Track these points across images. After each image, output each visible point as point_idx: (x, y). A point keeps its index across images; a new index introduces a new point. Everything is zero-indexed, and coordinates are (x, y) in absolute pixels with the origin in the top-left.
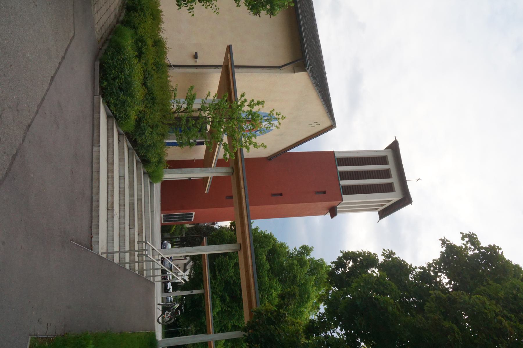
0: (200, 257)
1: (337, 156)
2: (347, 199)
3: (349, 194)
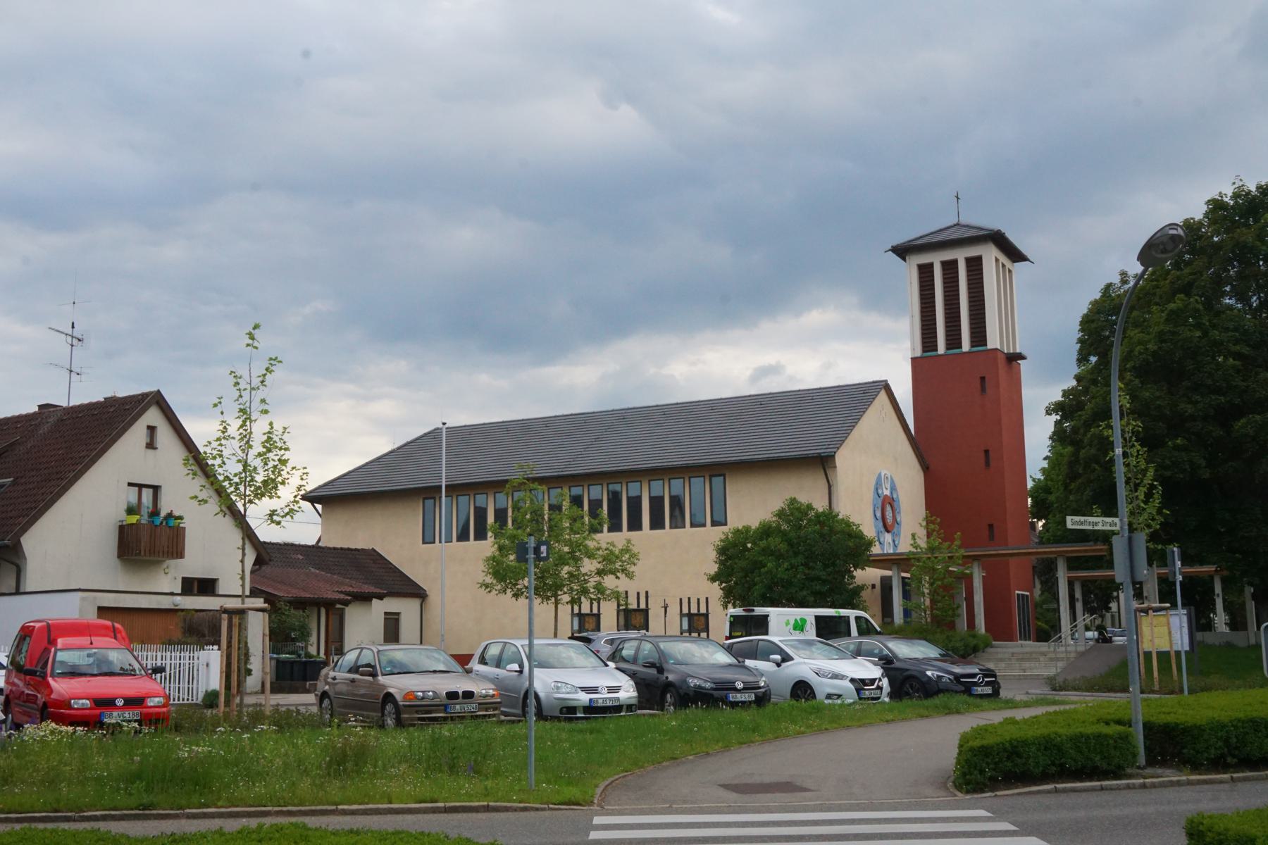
0: (1110, 565)
1: (918, 353)
2: (993, 341)
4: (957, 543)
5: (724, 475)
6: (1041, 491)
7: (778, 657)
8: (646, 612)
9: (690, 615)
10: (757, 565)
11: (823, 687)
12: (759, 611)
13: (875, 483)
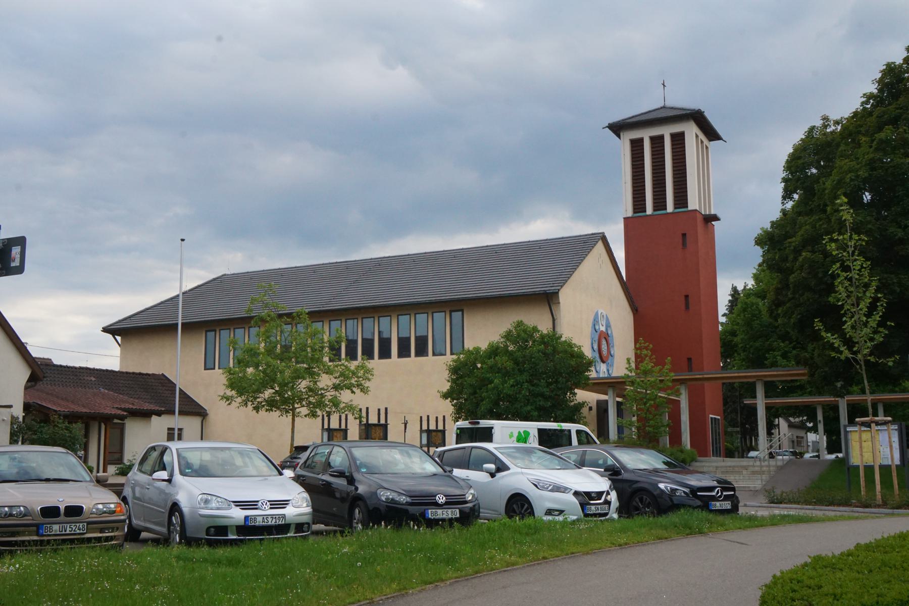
0: (768, 408)
1: (630, 213)
2: (693, 203)
3: (686, 188)
4: (668, 367)
5: (462, 311)
6: (729, 335)
7: (492, 466)
8: (385, 427)
9: (429, 431)
10: (484, 382)
11: (542, 500)
12: (484, 423)
13: (593, 312)
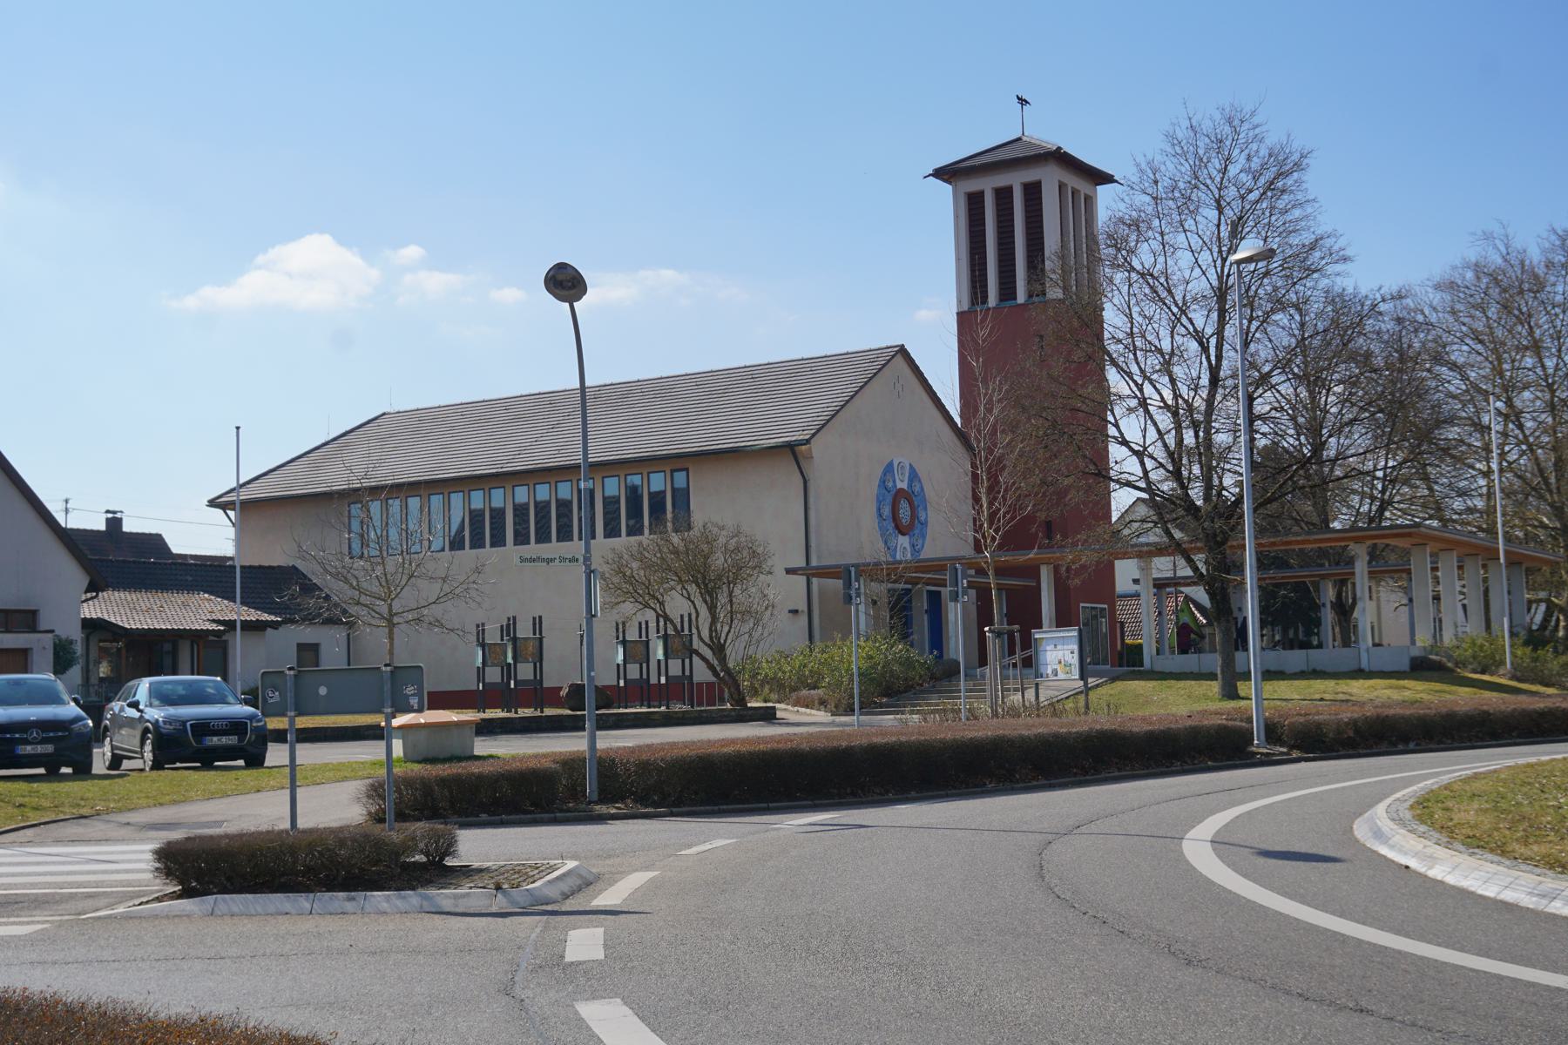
5: (687, 470)
